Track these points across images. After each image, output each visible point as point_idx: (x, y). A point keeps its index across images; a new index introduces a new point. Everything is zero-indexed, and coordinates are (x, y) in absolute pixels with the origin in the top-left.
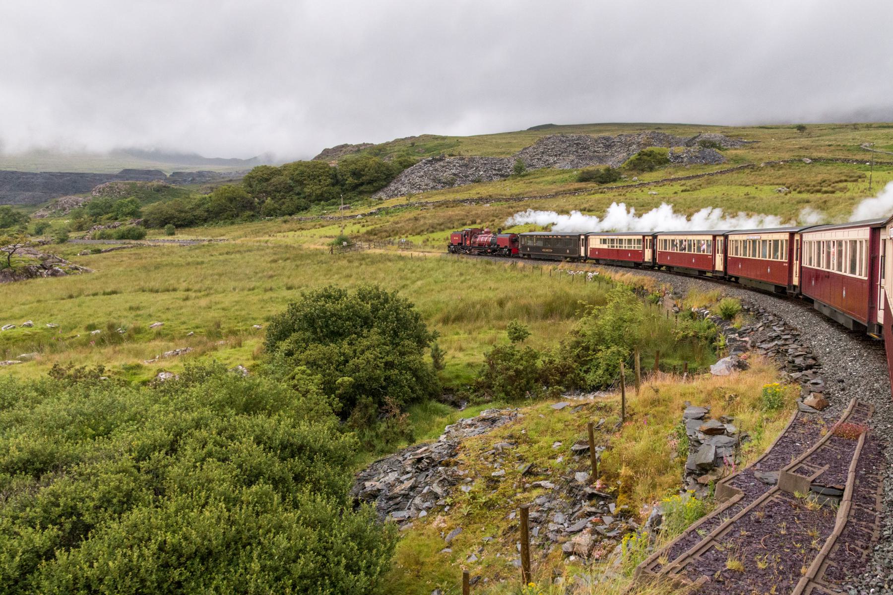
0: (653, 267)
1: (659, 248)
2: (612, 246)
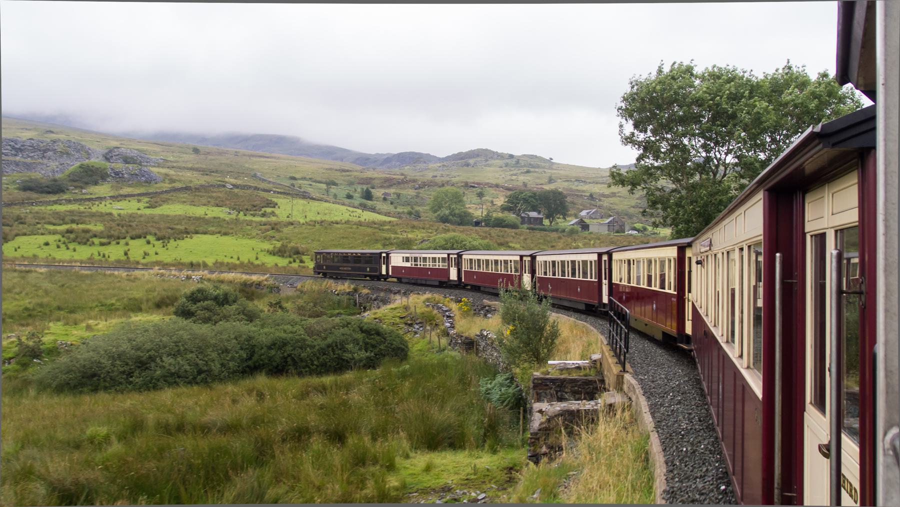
0: (458, 285)
1: (465, 267)
2: (415, 265)
